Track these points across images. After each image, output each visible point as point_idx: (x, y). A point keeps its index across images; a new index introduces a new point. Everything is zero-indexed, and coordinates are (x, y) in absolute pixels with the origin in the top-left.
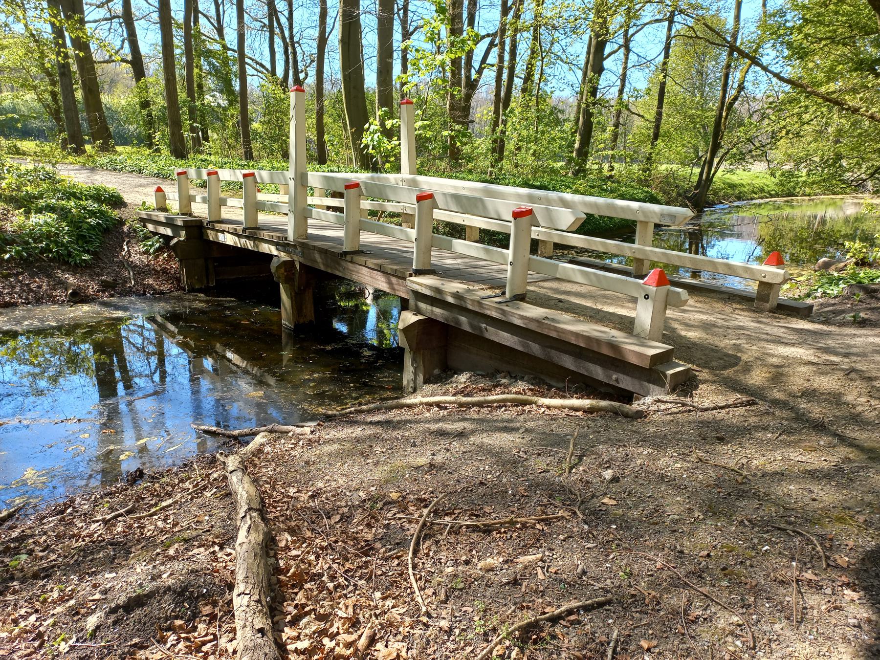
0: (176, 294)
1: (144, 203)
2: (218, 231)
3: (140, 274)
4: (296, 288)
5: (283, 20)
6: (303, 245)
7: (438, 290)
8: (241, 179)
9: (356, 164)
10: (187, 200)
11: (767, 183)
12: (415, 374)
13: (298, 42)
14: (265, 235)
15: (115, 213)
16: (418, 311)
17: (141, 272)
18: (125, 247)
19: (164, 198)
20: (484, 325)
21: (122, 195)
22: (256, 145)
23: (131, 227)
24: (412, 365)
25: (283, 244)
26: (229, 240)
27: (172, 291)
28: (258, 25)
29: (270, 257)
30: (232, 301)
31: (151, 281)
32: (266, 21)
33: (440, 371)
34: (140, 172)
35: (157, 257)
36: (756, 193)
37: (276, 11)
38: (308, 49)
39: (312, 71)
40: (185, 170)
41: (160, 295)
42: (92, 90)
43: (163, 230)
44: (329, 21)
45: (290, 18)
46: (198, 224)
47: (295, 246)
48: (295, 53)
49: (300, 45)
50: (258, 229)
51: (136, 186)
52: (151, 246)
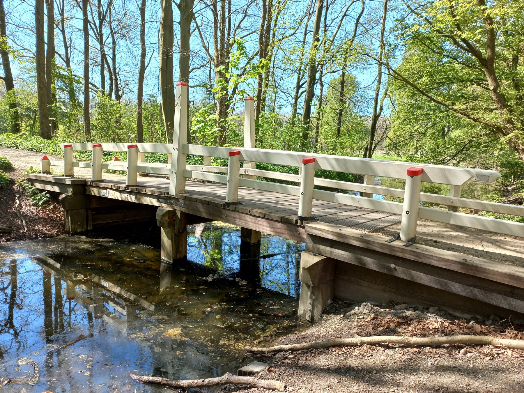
0: (62, 236)
1: (32, 168)
2: (100, 188)
3: (31, 222)
6: (185, 198)
7: (339, 235)
8: (126, 150)
10: (70, 166)
12: (313, 306)
13: (118, 73)
14: (148, 191)
15: (7, 176)
16: (318, 253)
17: (32, 220)
18: (17, 201)
19: (49, 164)
20: (392, 266)
21: (11, 162)
22: (93, 133)
23: (20, 185)
24: (311, 298)
25: (165, 197)
26: (113, 195)
27: (59, 235)
29: (154, 209)
30: (111, 242)
31: (40, 227)
33: (338, 303)
34: (17, 147)
35: (44, 208)
38: (124, 78)
41: (48, 239)
43: (49, 188)
45: (114, 60)
46: (83, 183)
47: (177, 199)
48: (116, 79)
50: (138, 186)
51: (17, 157)
52: (39, 200)
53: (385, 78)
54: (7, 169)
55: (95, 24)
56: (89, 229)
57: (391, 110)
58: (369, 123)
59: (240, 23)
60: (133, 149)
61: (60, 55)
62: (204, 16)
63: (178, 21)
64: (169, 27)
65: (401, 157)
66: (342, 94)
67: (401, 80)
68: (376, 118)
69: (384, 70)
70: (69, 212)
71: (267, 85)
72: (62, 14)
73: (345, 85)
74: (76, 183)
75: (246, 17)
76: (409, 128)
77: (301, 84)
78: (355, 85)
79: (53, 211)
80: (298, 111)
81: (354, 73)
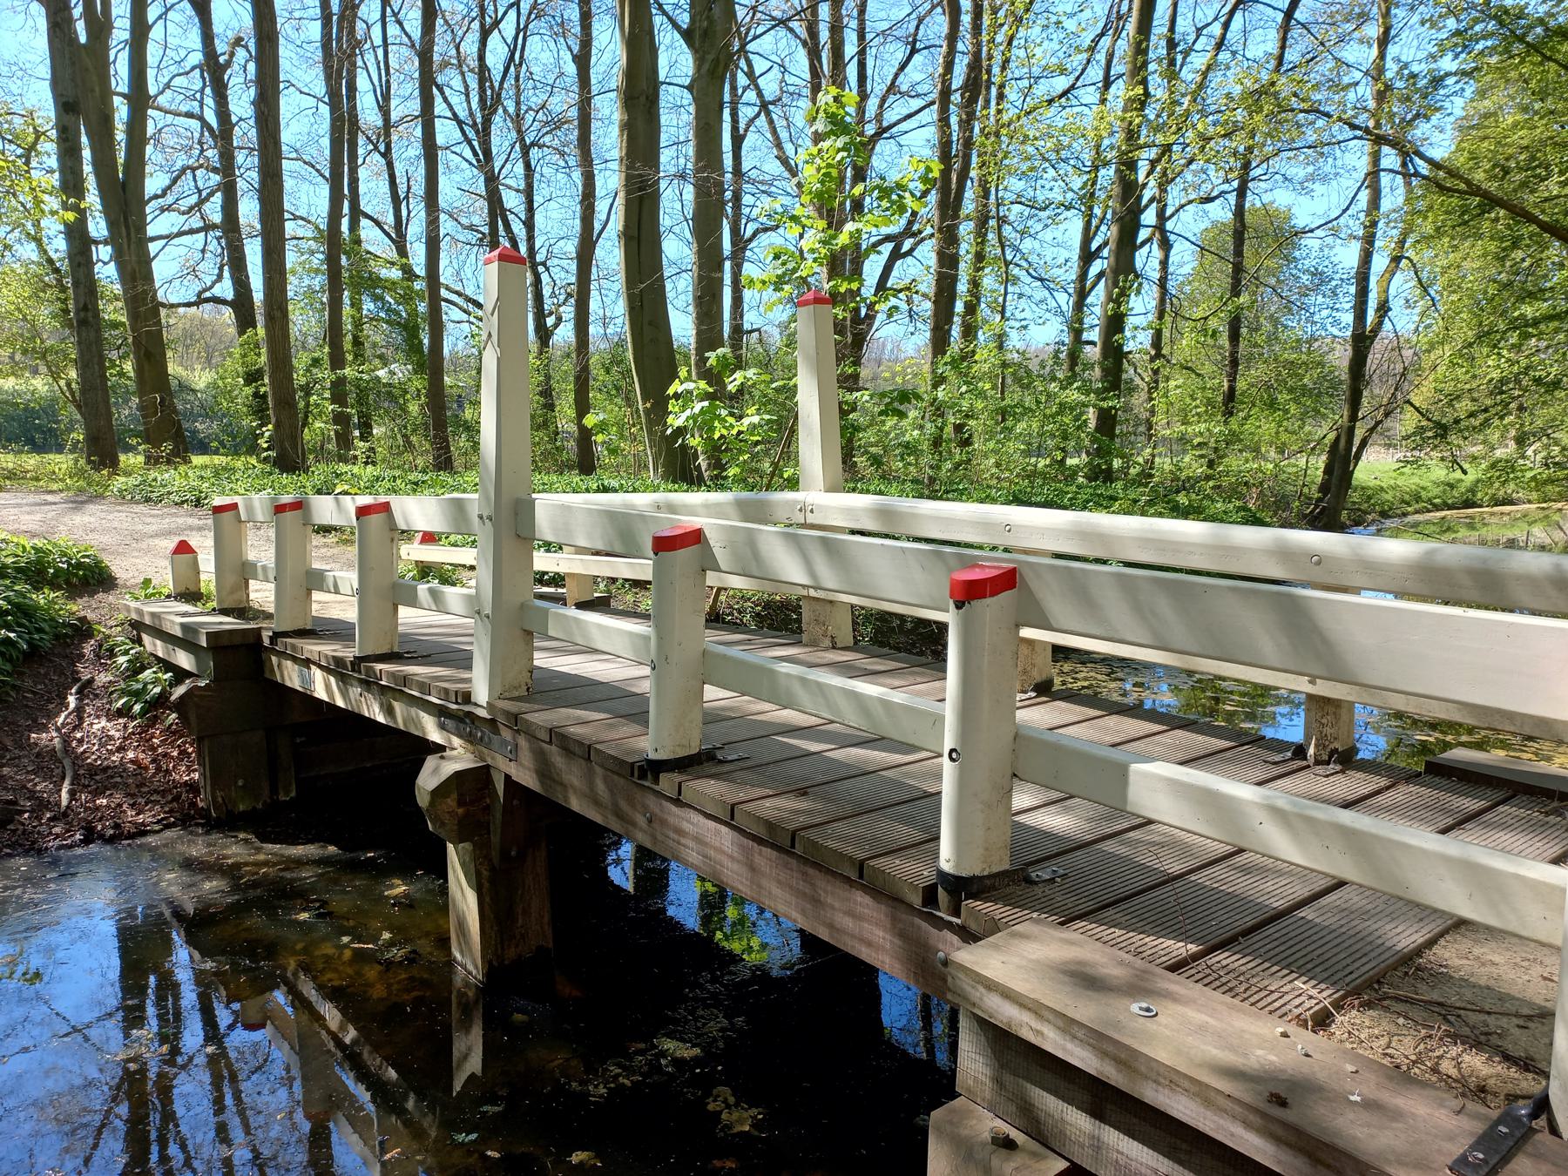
1: (147, 582)
4: (495, 854)
5: (518, 229)
9: (656, 469)
11: (1423, 483)
13: (544, 264)
18: (72, 701)
21: (107, 560)
28: (473, 237)
32: (486, 230)
36: (1408, 504)
37: (503, 211)
38: (563, 275)
39: (568, 312)
40: (382, 499)
42: (150, 351)
44: (601, 207)
45: (529, 224)
47: (493, 722)
49: (547, 269)
53: (1394, 195)
54: (88, 584)
55: (475, 124)
56: (282, 798)
57: (1417, 310)
58: (1341, 358)
59: (896, 76)
60: (375, 519)
61: (378, 223)
62: (776, 57)
63: (687, 82)
64: (643, 99)
65: (1465, 472)
66: (1238, 269)
67: (1463, 197)
68: (1362, 341)
69: (1390, 158)
70: (206, 742)
71: (980, 257)
72: (385, 110)
73: (1249, 245)
74: (225, 642)
75: (917, 58)
76: (1492, 367)
77: (1094, 246)
78: (1286, 237)
79: (174, 733)
80: (1085, 336)
81: (1281, 198)
